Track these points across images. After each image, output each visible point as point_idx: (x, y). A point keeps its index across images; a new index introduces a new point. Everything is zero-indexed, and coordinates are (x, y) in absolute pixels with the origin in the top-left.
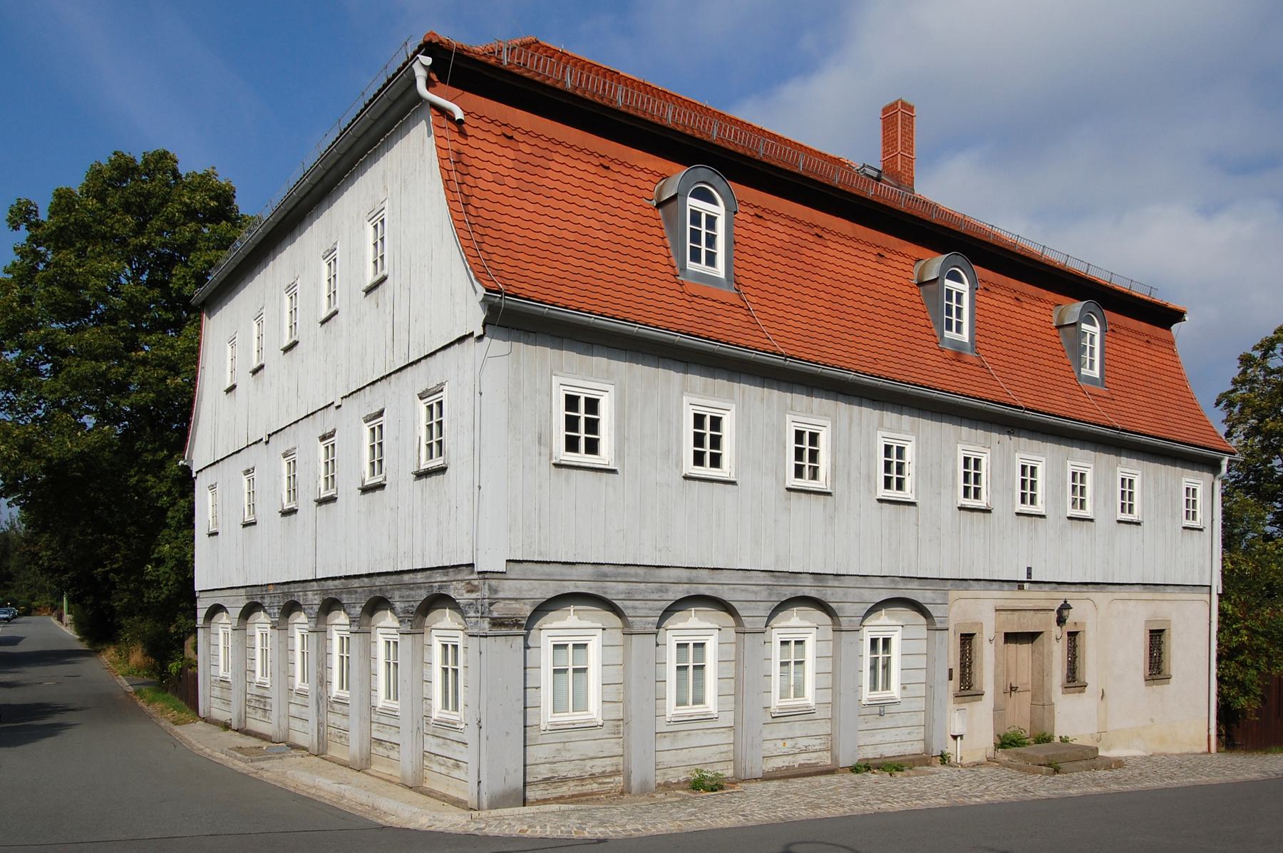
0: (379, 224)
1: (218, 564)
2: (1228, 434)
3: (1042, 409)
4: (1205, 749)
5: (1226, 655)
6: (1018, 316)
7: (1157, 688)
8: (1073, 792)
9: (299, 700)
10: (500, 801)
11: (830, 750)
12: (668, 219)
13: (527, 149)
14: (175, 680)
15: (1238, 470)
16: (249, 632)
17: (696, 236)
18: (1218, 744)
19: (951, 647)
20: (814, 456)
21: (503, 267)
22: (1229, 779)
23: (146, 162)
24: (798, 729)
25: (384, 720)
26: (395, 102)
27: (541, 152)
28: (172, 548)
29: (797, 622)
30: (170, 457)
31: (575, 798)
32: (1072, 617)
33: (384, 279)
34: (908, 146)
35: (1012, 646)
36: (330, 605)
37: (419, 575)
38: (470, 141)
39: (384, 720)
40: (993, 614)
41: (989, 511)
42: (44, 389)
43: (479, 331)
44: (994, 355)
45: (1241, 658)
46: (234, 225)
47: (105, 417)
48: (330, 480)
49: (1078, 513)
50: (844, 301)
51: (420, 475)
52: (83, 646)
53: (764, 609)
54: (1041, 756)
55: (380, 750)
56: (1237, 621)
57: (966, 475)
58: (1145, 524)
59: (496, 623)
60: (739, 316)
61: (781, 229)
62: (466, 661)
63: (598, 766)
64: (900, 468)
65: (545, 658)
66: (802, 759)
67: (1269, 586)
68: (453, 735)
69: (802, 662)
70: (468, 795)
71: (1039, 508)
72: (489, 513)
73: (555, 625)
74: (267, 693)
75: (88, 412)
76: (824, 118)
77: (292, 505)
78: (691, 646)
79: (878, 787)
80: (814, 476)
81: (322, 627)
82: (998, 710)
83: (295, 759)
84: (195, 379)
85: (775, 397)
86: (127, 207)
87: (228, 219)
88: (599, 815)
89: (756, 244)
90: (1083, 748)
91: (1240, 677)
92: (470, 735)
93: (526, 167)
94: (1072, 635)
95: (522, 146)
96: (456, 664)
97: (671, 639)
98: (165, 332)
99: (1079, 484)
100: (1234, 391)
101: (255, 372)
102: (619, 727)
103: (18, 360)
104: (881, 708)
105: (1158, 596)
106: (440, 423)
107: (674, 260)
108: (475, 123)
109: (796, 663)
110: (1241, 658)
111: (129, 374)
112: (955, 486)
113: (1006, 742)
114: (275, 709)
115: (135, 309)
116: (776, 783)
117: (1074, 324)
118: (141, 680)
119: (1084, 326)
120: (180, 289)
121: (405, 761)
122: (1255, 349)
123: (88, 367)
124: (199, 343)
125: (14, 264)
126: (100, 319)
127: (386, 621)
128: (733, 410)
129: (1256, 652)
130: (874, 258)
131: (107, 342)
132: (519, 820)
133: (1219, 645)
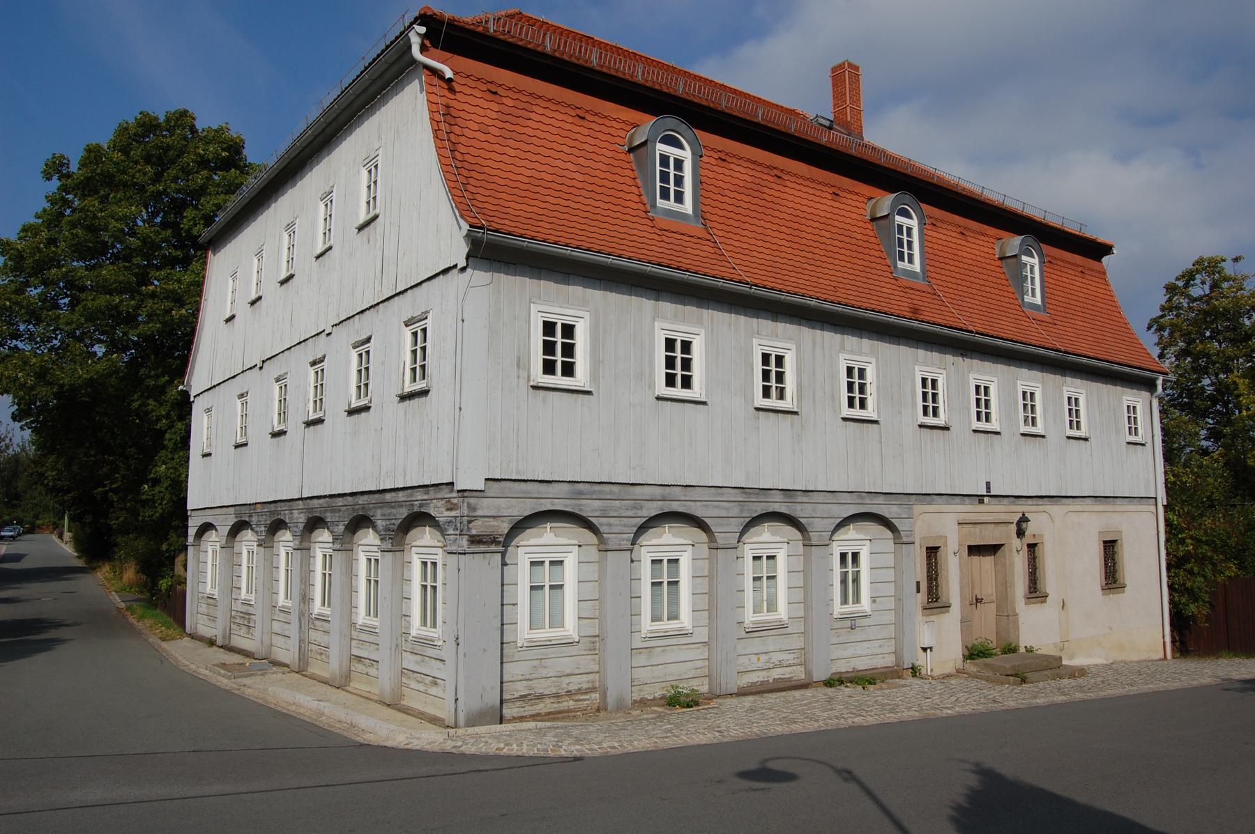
0: (373, 168)
1: (209, 484)
2: (1161, 356)
3: (991, 333)
4: (1161, 655)
5: (1175, 564)
6: (964, 248)
7: (1113, 597)
8: (1040, 701)
9: (282, 617)
10: (476, 719)
11: (804, 664)
12: (638, 161)
13: (511, 103)
14: (164, 595)
15: (1172, 388)
16: (236, 549)
17: (665, 177)
18: (1173, 650)
19: (918, 559)
20: (780, 377)
21: (486, 205)
22: (1185, 684)
23: (168, 120)
24: (772, 643)
25: (364, 637)
26: (392, 65)
27: (522, 105)
28: (168, 469)
29: (768, 537)
30: (171, 382)
31: (550, 716)
32: (1030, 529)
33: (376, 217)
34: (856, 98)
35: (976, 559)
36: (315, 523)
37: (401, 494)
38: (458, 96)
39: (364, 637)
40: (956, 527)
41: (948, 429)
42: (62, 321)
43: (462, 263)
44: (944, 284)
45: (1189, 566)
46: (242, 172)
47: (115, 346)
48: (319, 403)
49: (1030, 429)
50: (804, 235)
51: (404, 398)
52: (80, 563)
53: (736, 525)
54: (1008, 666)
55: (360, 667)
56: (1182, 531)
57: (925, 395)
58: (1092, 440)
59: (475, 540)
60: (705, 248)
61: (743, 170)
62: (445, 578)
63: (575, 683)
64: (862, 388)
65: (522, 575)
66: (776, 674)
67: (1209, 498)
68: (431, 652)
69: (774, 577)
70: (446, 713)
71: (994, 425)
72: (470, 433)
73: (532, 542)
74: (251, 610)
75: (100, 341)
76: (777, 75)
77: (282, 427)
78: (665, 562)
79: (851, 701)
80: (781, 396)
81: (306, 544)
82: (965, 622)
83: (276, 675)
84: (198, 310)
85: (742, 322)
86: (148, 159)
87: (237, 167)
88: (576, 732)
89: (721, 184)
90: (1047, 658)
91: (1189, 584)
92: (448, 652)
93: (509, 118)
94: (1032, 547)
95: (505, 101)
96: (435, 580)
97: (645, 555)
98: (173, 268)
99: (1029, 402)
100: (1162, 317)
101: (253, 303)
102: (595, 643)
103: (40, 295)
104: (853, 622)
105: (1109, 508)
106: (424, 349)
107: (645, 198)
108: (463, 81)
109: (768, 578)
110: (1189, 566)
111: (138, 307)
112: (914, 405)
113: (974, 653)
114: (259, 626)
115: (148, 248)
116: (750, 698)
117: (1015, 256)
118: (132, 597)
119: (1024, 258)
120: (190, 229)
121: (384, 679)
122: (1177, 279)
123: (103, 300)
124: (204, 277)
125: (45, 210)
126: (116, 257)
127: (368, 539)
128: (703, 334)
129: (1202, 560)
130: (829, 197)
131: (121, 278)
132: (496, 738)
133: (1168, 554)
